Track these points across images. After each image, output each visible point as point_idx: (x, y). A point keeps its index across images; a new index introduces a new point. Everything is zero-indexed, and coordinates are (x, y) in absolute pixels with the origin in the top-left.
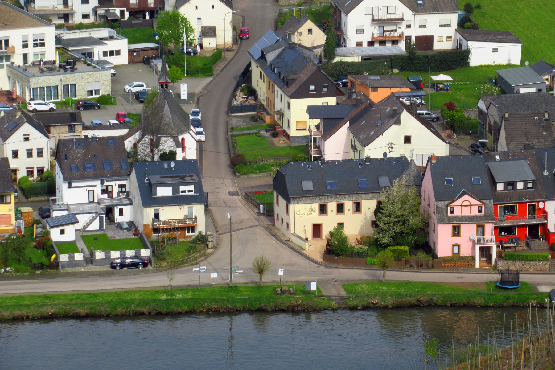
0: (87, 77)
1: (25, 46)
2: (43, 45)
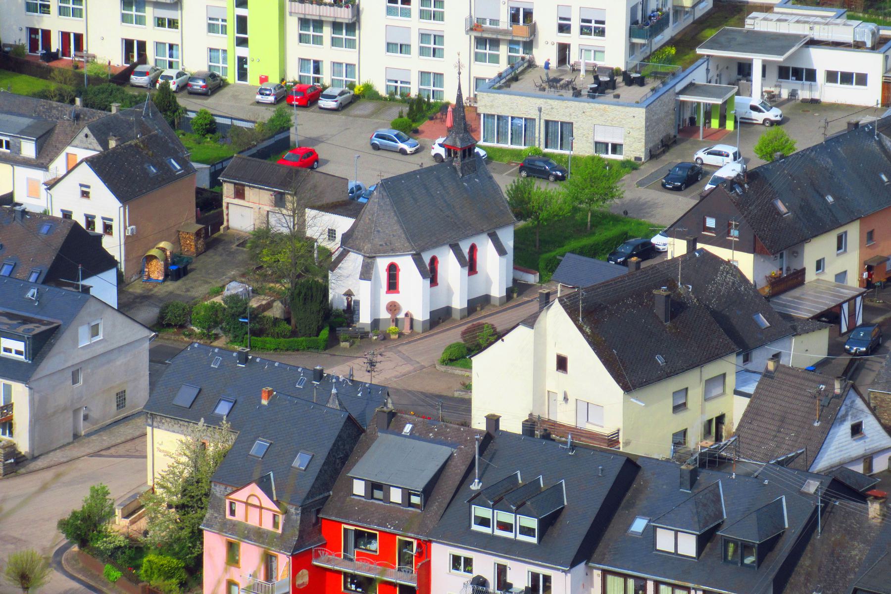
0: (593, 113)
1: (564, 28)
2: (601, 33)
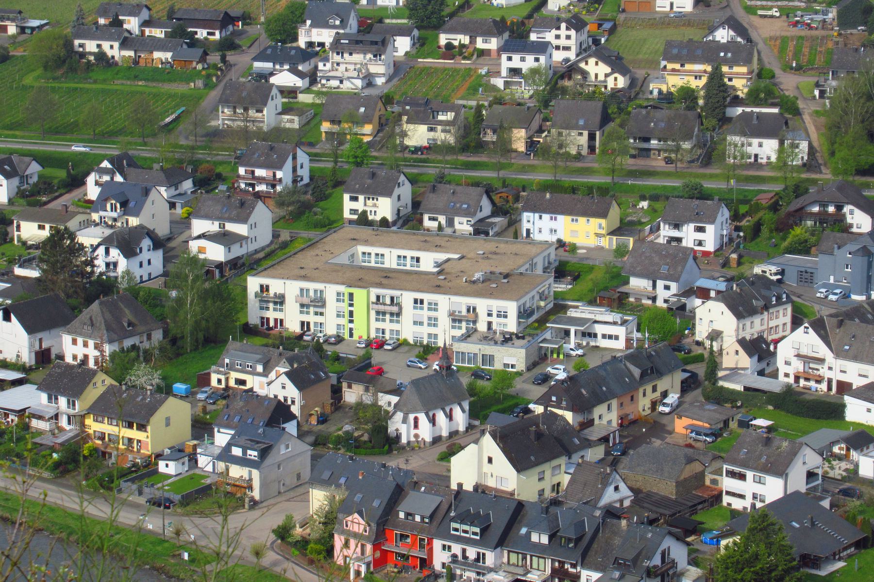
1: (490, 315)
2: (506, 317)
